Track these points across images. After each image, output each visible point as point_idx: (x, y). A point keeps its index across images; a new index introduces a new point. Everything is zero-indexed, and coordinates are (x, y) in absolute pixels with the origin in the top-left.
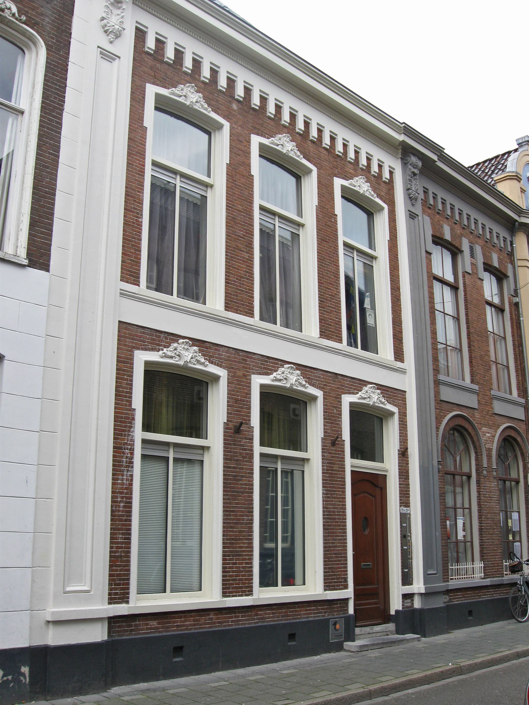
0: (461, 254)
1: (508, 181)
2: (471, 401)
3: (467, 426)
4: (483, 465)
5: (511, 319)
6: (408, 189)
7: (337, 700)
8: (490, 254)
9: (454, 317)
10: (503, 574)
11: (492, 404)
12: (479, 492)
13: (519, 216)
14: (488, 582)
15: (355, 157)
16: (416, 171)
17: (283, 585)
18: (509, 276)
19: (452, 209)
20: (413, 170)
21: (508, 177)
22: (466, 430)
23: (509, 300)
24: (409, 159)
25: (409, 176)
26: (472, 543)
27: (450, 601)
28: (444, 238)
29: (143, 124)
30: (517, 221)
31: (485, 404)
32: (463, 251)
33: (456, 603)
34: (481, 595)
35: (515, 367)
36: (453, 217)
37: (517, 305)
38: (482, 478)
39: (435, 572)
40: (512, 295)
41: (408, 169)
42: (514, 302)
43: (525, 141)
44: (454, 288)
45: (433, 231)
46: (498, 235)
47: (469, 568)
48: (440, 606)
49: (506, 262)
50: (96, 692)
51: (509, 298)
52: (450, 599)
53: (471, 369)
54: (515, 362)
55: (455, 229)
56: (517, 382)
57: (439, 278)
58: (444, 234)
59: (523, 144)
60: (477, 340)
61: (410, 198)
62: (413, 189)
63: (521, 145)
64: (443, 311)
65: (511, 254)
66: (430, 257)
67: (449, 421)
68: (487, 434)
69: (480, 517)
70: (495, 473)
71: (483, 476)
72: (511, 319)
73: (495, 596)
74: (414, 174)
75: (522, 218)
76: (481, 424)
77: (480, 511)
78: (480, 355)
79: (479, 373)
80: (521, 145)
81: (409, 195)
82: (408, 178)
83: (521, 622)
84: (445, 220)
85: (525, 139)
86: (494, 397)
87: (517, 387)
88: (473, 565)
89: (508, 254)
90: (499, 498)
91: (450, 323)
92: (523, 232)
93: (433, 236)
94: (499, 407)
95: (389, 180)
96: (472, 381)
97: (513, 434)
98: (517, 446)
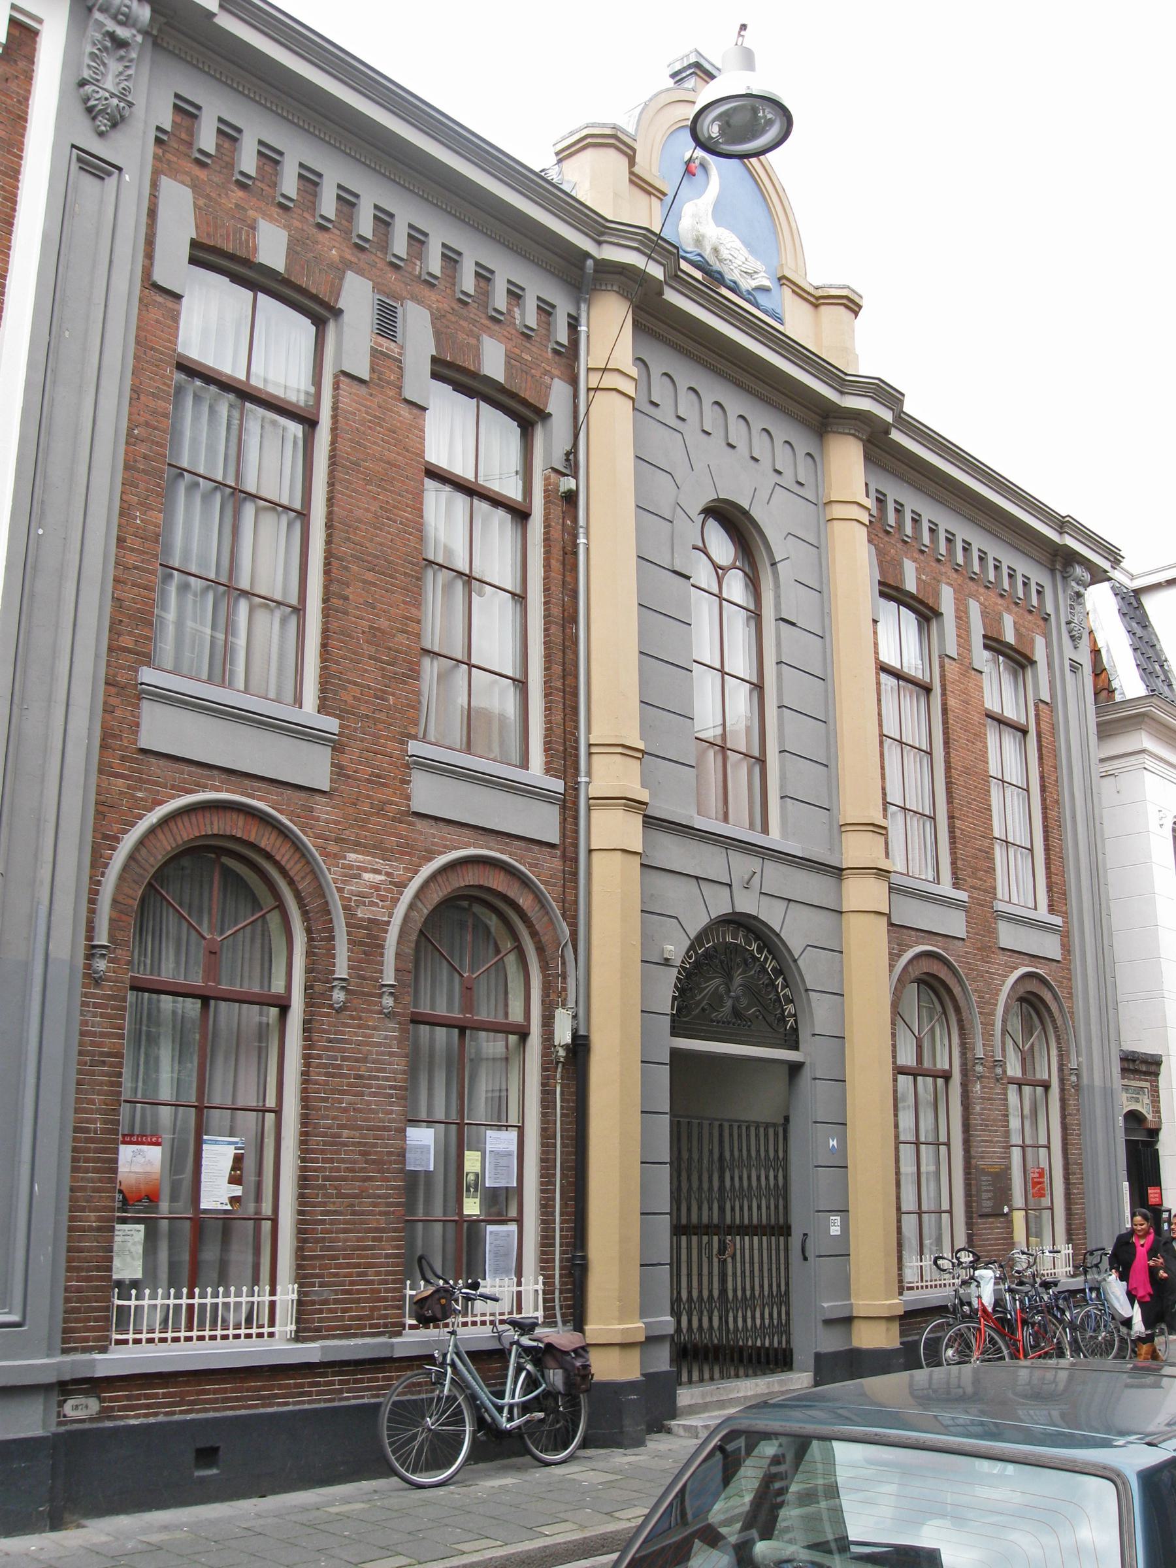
0: (543, 426)
1: (589, 154)
2: (955, 924)
3: (943, 973)
4: (333, 972)
5: (547, 540)
6: (83, 83)
7: (508, 1558)
8: (473, 341)
9: (513, 594)
10: (108, 1338)
11: (408, 782)
12: (306, 1058)
13: (599, 243)
14: (312, 1351)
18: (550, 415)
19: (916, 521)
21: (589, 140)
22: (269, 857)
23: (545, 485)
25: (95, 44)
26: (275, 1221)
27: (105, 1413)
28: (482, 373)
30: (587, 255)
31: (369, 781)
32: (1035, 662)
33: (133, 1422)
34: (277, 1396)
35: (545, 682)
36: (899, 530)
37: (571, 498)
38: (328, 1015)
39: (15, 1318)
40: (553, 469)
41: (91, 22)
42: (562, 489)
43: (689, 66)
44: (520, 515)
46: (998, 564)
47: (203, 1307)
48: (30, 1434)
49: (546, 372)
51: (547, 478)
52: (103, 1410)
53: (322, 668)
54: (546, 669)
55: (317, 242)
56: (547, 729)
57: (223, 379)
58: (902, 580)
59: (684, 75)
60: (365, 582)
61: (90, 110)
62: (1076, 621)
63: (678, 78)
64: (899, 738)
65: (569, 354)
66: (176, 307)
67: (911, 962)
68: (366, 876)
69: (304, 1137)
70: (388, 1001)
71: (331, 1006)
72: (545, 540)
73: (348, 1398)
75: (605, 246)
76: (338, 840)
77: (305, 1120)
78: (371, 627)
79: (355, 683)
80: (678, 78)
81: (87, 99)
82: (89, 49)
83: (548, 1464)
84: (275, 211)
85: (688, 60)
86: (416, 763)
87: (545, 743)
88: (921, 1261)
89: (555, 351)
90: (405, 1081)
91: (1014, 800)
92: (617, 292)
93: (985, 636)
94: (1008, 936)
96: (322, 708)
97: (1033, 986)
98: (1047, 1016)
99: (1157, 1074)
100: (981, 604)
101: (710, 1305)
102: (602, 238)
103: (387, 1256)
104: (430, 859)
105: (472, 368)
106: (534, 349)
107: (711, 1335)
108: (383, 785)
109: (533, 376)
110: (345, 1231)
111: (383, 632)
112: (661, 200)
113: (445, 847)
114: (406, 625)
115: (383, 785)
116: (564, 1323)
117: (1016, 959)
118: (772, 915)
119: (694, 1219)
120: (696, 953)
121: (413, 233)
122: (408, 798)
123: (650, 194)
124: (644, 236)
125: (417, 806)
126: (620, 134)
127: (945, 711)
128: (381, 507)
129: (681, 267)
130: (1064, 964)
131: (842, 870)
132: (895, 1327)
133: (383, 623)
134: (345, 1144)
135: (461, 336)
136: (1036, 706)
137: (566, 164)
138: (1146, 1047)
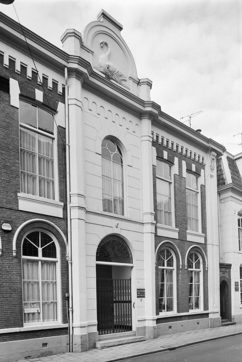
4: (12, 249)
8: (33, 90)
15: (162, 142)
16: (214, 158)
17: (98, 266)
20: (213, 157)
24: (211, 153)
29: (9, 101)
30: (65, 66)
44: (170, 183)
45: (187, 168)
49: (57, 100)
50: (230, 290)
74: (213, 159)
94: (189, 238)
95: (62, 93)
99: (230, 268)
100: (186, 162)
101: (126, 316)
102: (68, 61)
103: (18, 310)
104: (25, 221)
105: (33, 98)
106: (53, 94)
107: (122, 323)
108: (10, 204)
109: (52, 101)
110: (5, 305)
111: (8, 166)
112: (92, 54)
113: (29, 218)
114: (15, 164)
115: (10, 204)
116: (153, 317)
117: (190, 244)
118: (123, 234)
119: (125, 300)
120: (104, 242)
121: (53, 81)
122: (18, 207)
123: (89, 52)
124: (79, 59)
125: (20, 209)
126: (76, 32)
127: (175, 187)
128: (5, 134)
129: (94, 70)
130: (205, 245)
131: (144, 224)
132: (155, 321)
133: (8, 164)
134: (4, 286)
135: (29, 89)
136: (174, 177)
137: (64, 43)
138: (228, 262)
